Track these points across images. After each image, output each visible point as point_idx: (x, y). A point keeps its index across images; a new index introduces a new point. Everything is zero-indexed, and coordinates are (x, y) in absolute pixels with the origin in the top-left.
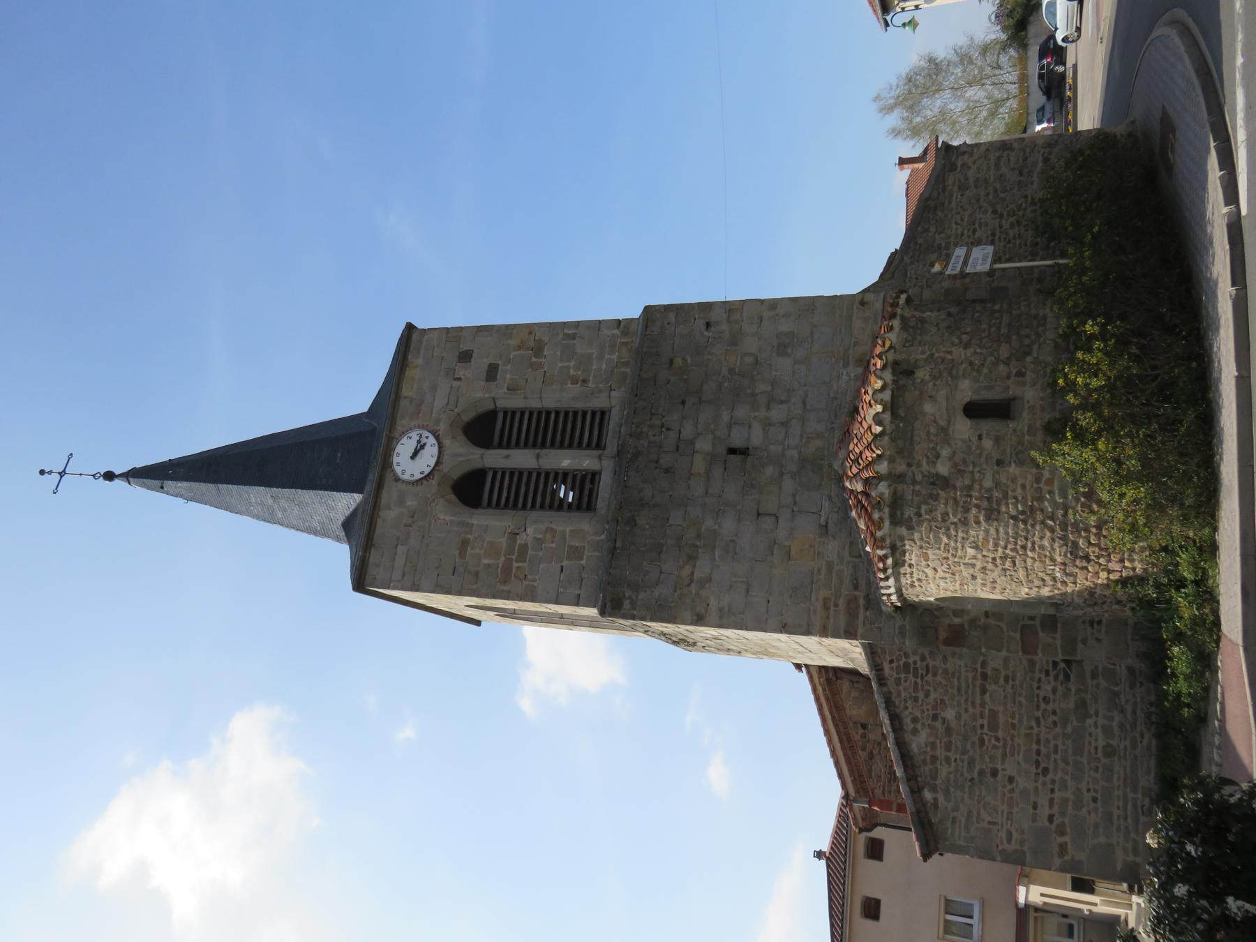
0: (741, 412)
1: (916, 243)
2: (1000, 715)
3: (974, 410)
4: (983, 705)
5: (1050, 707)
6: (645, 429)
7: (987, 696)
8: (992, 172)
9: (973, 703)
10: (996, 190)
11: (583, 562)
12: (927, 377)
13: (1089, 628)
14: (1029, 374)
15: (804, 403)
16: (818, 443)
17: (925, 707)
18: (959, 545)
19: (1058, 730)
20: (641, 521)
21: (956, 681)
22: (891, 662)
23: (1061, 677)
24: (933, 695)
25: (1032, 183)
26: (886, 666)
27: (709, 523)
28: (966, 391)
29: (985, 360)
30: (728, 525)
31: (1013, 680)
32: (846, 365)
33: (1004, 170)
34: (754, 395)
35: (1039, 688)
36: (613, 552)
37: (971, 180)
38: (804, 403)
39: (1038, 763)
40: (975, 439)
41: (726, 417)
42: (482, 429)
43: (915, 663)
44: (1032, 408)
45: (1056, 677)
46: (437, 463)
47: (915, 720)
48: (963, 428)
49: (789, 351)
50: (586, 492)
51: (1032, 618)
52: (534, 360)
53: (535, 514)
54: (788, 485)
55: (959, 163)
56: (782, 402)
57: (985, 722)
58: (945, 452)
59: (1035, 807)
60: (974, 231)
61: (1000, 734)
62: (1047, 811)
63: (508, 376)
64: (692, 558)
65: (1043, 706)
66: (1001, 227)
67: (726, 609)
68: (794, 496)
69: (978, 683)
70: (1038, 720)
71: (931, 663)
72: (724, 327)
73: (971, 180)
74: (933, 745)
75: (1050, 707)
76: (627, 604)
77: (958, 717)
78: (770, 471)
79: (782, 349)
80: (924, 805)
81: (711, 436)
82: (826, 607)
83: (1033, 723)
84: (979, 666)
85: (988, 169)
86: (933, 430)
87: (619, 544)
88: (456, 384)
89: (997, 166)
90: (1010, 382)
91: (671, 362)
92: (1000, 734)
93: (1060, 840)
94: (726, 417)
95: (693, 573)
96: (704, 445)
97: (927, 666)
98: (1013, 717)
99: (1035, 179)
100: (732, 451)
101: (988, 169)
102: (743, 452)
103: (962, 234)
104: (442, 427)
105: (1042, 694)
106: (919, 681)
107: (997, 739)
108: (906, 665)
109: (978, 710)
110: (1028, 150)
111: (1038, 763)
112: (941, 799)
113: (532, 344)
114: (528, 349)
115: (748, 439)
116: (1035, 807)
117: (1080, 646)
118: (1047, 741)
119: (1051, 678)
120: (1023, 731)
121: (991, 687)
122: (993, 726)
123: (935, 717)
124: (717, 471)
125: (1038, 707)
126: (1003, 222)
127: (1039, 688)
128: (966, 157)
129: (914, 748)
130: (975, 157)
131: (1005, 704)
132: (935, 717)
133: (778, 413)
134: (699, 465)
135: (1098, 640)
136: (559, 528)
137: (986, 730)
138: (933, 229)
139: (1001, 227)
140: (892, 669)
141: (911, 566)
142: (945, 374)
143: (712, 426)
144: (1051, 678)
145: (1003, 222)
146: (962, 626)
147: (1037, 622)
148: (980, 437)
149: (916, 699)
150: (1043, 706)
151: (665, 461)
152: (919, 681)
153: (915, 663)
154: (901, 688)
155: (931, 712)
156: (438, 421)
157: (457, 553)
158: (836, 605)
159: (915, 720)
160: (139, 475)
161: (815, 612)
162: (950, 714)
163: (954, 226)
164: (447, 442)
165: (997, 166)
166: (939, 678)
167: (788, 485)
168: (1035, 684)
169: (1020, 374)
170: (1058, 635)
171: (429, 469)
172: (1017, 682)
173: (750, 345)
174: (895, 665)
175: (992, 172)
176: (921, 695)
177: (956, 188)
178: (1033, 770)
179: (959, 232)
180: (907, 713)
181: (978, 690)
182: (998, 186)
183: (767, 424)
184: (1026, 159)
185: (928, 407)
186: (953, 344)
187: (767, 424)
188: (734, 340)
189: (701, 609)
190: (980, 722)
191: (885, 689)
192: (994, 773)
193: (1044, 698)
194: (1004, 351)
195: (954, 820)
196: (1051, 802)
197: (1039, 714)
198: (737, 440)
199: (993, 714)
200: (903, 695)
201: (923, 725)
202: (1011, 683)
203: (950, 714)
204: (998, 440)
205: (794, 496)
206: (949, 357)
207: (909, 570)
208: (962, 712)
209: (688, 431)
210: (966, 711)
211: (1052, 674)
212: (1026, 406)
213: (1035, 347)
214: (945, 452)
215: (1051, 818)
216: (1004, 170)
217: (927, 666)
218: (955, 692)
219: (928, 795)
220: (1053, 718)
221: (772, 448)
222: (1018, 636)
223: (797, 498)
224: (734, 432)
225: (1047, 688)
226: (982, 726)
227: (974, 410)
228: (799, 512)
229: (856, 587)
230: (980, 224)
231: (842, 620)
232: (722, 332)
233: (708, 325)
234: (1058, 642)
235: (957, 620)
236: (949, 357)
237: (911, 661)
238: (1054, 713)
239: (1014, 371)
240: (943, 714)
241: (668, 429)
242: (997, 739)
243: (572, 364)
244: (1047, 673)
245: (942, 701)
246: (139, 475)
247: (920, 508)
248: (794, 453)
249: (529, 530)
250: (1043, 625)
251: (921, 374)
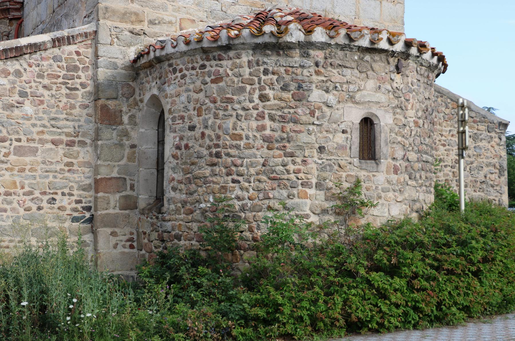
2: (32, 158)
3: (368, 124)
4: (42, 142)
5: (44, 204)
7: (49, 146)
9: (42, 132)
10: (472, 163)
12: (395, 85)
13: (125, 238)
14: (396, 177)
17: (33, 84)
19: (22, 211)
21: (64, 116)
22: (78, 53)
23: (76, 214)
24: (46, 93)
25: (475, 191)
26: (72, 48)
28: (385, 120)
29: (406, 139)
31: (69, 171)
33: (486, 169)
35: (63, 194)
37: (480, 144)
40: (343, 126)
43: (79, 77)
45: (75, 210)
48: (354, 116)
51: (132, 188)
55: (493, 134)
57: (24, 143)
58: (331, 98)
60: (444, 145)
61: (12, 158)
65: (46, 198)
66: (446, 166)
69: (64, 138)
70: (30, 193)
71: (79, 93)
73: (480, 144)
75: (44, 204)
77: (28, 118)
83: (27, 189)
84: (80, 138)
85: (487, 158)
86: (352, 87)
90: (390, 160)
92: (12, 158)
97: (76, 89)
98: (31, 170)
99: (478, 193)
101: (487, 158)
103: (442, 135)
105: (58, 197)
106: (61, 80)
108: (76, 69)
109: (36, 136)
117: (109, 230)
118: (10, 203)
119: (74, 205)
120: (18, 180)
121: (61, 150)
122: (19, 151)
123: (23, 94)
125: (44, 193)
126: (449, 168)
127: (63, 194)
128: (497, 140)
131: (44, 163)
135: (115, 246)
137: (15, 143)
138: (447, 111)
139: (446, 166)
140: (70, 53)
141: (203, 66)
144: (74, 205)
145: (449, 168)
146: (121, 123)
147: (129, 192)
148: (344, 132)
149: (40, 76)
150: (46, 198)
152: (61, 80)
153: (79, 77)
154: (51, 61)
155: (28, 90)
159: (18, 74)
162: (28, 108)
163: (448, 129)
166: (64, 100)
168: (66, 191)
169: (396, 171)
170: (117, 211)
172: (67, 174)
174: (76, 57)
175: (485, 160)
176: (46, 81)
177: (476, 131)
179: (444, 133)
180: (25, 66)
181: (57, 137)
182: (475, 165)
184: (492, 186)
185: (371, 84)
186: (417, 111)
190: (24, 138)
191: (49, 45)
193: (54, 199)
194: (413, 156)
197: (37, 194)
199: (34, 151)
200: (45, 63)
201: (14, 83)
202: (67, 168)
203: (28, 108)
204: (341, 147)
206: (410, 106)
207: (197, 65)
208: (33, 121)
210: (34, 125)
211: (79, 206)
212: (371, 174)
213: (414, 183)
214: (331, 98)
216: (486, 169)
217: (76, 89)
218: (53, 115)
220: (34, 207)
222: (115, 174)
225: (65, 201)
226: (19, 140)
227: (368, 124)
229: (152, 23)
230: (448, 150)
234: (111, 211)
235: (125, 119)
237: (80, 73)
238: (39, 208)
240: (27, 102)
244: (78, 202)
245: (42, 102)
247: (273, 73)
250: (126, 197)
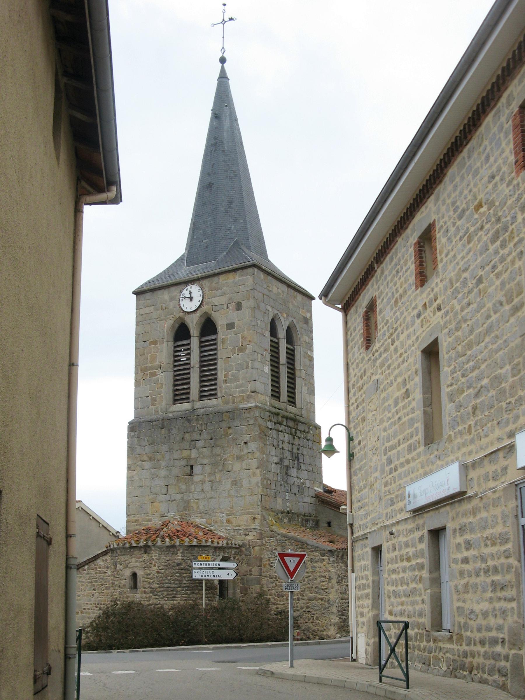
0: (208, 468)
1: (286, 540)
3: (134, 575)
6: (200, 422)
8: (318, 574)
11: (150, 407)
15: (211, 498)
16: (195, 507)
18: (414, 562)
20: (163, 431)
27: (163, 464)
28: (140, 573)
30: (163, 473)
32: (227, 515)
33: (319, 580)
34: (215, 473)
36: (151, 421)
37: (315, 564)
38: (211, 498)
39: (98, 604)
41: (205, 461)
42: (209, 327)
44: (134, 597)
46: (189, 313)
47: (106, 560)
48: (128, 573)
49: (234, 486)
50: (283, 358)
52: (237, 348)
53: (171, 374)
54: (179, 496)
56: (212, 487)
59: (87, 604)
62: (86, 608)
63: (229, 336)
64: (151, 459)
67: (133, 479)
68: (175, 500)
72: (246, 451)
74: (100, 568)
76: (132, 434)
78: (184, 487)
79: (235, 483)
80: (84, 566)
81: (197, 456)
82: (136, 521)
85: (320, 572)
87: (154, 423)
88: (225, 306)
89: (321, 576)
91: (230, 428)
93: (80, 612)
94: (205, 461)
95: (145, 461)
96: (194, 454)
100: (192, 467)
102: (191, 474)
104: (205, 308)
107: (103, 590)
110: (327, 591)
111: (98, 604)
112: (86, 572)
113: (244, 344)
114: (242, 343)
115: (196, 475)
116: (87, 604)
124: (184, 462)
129: (98, 561)
130: (327, 565)
132: (108, 568)
133: (207, 486)
134: (185, 453)
136: (163, 390)
142: (145, 565)
143: (201, 456)
151: (187, 436)
156: (207, 304)
157: (152, 340)
158: (137, 525)
160: (223, 77)
161: (134, 517)
164: (198, 314)
165: (321, 576)
167: (179, 496)
171: (201, 298)
173: (237, 466)
178: (97, 603)
183: (202, 482)
185: (134, 560)
187: (202, 482)
188: (239, 458)
189: (132, 469)
190: (108, 584)
192: (94, 590)
195: (81, 577)
196: (89, 609)
198: (197, 469)
204: (124, 585)
205: (175, 500)
209: (200, 444)
215: (84, 609)
219: (86, 567)
221: (193, 486)
223: (174, 502)
224: (199, 467)
227: (134, 575)
228: (169, 504)
231: (132, 528)
232: (243, 451)
233: (245, 443)
236: (152, 566)
239: (146, 590)
241: (200, 434)
242: (103, 590)
243: (234, 371)
246: (223, 77)
248: (191, 498)
249: (162, 374)
251: (145, 556)
